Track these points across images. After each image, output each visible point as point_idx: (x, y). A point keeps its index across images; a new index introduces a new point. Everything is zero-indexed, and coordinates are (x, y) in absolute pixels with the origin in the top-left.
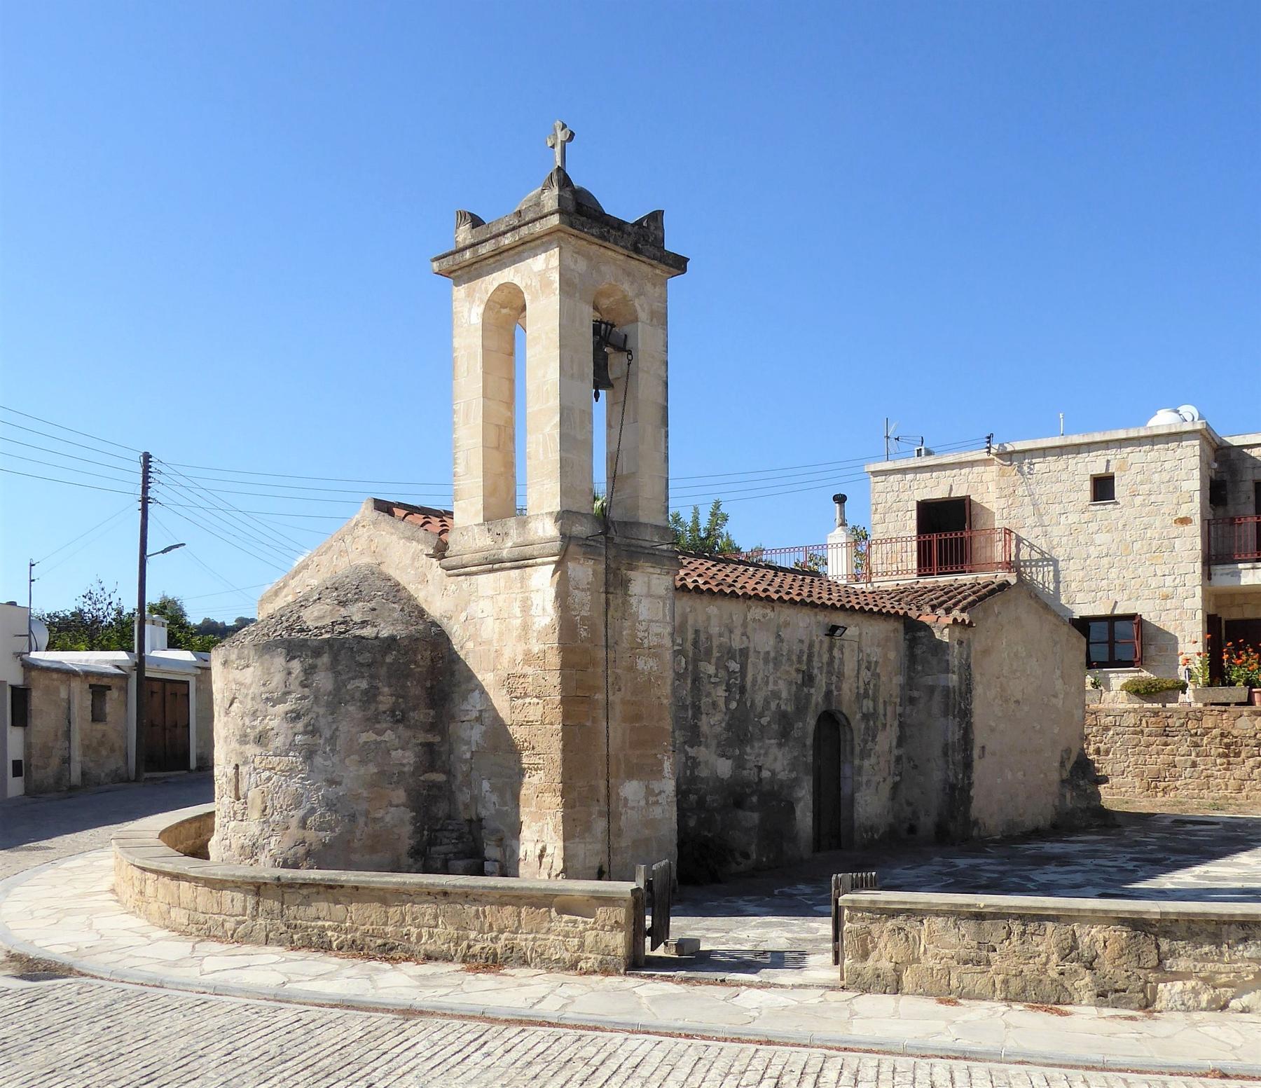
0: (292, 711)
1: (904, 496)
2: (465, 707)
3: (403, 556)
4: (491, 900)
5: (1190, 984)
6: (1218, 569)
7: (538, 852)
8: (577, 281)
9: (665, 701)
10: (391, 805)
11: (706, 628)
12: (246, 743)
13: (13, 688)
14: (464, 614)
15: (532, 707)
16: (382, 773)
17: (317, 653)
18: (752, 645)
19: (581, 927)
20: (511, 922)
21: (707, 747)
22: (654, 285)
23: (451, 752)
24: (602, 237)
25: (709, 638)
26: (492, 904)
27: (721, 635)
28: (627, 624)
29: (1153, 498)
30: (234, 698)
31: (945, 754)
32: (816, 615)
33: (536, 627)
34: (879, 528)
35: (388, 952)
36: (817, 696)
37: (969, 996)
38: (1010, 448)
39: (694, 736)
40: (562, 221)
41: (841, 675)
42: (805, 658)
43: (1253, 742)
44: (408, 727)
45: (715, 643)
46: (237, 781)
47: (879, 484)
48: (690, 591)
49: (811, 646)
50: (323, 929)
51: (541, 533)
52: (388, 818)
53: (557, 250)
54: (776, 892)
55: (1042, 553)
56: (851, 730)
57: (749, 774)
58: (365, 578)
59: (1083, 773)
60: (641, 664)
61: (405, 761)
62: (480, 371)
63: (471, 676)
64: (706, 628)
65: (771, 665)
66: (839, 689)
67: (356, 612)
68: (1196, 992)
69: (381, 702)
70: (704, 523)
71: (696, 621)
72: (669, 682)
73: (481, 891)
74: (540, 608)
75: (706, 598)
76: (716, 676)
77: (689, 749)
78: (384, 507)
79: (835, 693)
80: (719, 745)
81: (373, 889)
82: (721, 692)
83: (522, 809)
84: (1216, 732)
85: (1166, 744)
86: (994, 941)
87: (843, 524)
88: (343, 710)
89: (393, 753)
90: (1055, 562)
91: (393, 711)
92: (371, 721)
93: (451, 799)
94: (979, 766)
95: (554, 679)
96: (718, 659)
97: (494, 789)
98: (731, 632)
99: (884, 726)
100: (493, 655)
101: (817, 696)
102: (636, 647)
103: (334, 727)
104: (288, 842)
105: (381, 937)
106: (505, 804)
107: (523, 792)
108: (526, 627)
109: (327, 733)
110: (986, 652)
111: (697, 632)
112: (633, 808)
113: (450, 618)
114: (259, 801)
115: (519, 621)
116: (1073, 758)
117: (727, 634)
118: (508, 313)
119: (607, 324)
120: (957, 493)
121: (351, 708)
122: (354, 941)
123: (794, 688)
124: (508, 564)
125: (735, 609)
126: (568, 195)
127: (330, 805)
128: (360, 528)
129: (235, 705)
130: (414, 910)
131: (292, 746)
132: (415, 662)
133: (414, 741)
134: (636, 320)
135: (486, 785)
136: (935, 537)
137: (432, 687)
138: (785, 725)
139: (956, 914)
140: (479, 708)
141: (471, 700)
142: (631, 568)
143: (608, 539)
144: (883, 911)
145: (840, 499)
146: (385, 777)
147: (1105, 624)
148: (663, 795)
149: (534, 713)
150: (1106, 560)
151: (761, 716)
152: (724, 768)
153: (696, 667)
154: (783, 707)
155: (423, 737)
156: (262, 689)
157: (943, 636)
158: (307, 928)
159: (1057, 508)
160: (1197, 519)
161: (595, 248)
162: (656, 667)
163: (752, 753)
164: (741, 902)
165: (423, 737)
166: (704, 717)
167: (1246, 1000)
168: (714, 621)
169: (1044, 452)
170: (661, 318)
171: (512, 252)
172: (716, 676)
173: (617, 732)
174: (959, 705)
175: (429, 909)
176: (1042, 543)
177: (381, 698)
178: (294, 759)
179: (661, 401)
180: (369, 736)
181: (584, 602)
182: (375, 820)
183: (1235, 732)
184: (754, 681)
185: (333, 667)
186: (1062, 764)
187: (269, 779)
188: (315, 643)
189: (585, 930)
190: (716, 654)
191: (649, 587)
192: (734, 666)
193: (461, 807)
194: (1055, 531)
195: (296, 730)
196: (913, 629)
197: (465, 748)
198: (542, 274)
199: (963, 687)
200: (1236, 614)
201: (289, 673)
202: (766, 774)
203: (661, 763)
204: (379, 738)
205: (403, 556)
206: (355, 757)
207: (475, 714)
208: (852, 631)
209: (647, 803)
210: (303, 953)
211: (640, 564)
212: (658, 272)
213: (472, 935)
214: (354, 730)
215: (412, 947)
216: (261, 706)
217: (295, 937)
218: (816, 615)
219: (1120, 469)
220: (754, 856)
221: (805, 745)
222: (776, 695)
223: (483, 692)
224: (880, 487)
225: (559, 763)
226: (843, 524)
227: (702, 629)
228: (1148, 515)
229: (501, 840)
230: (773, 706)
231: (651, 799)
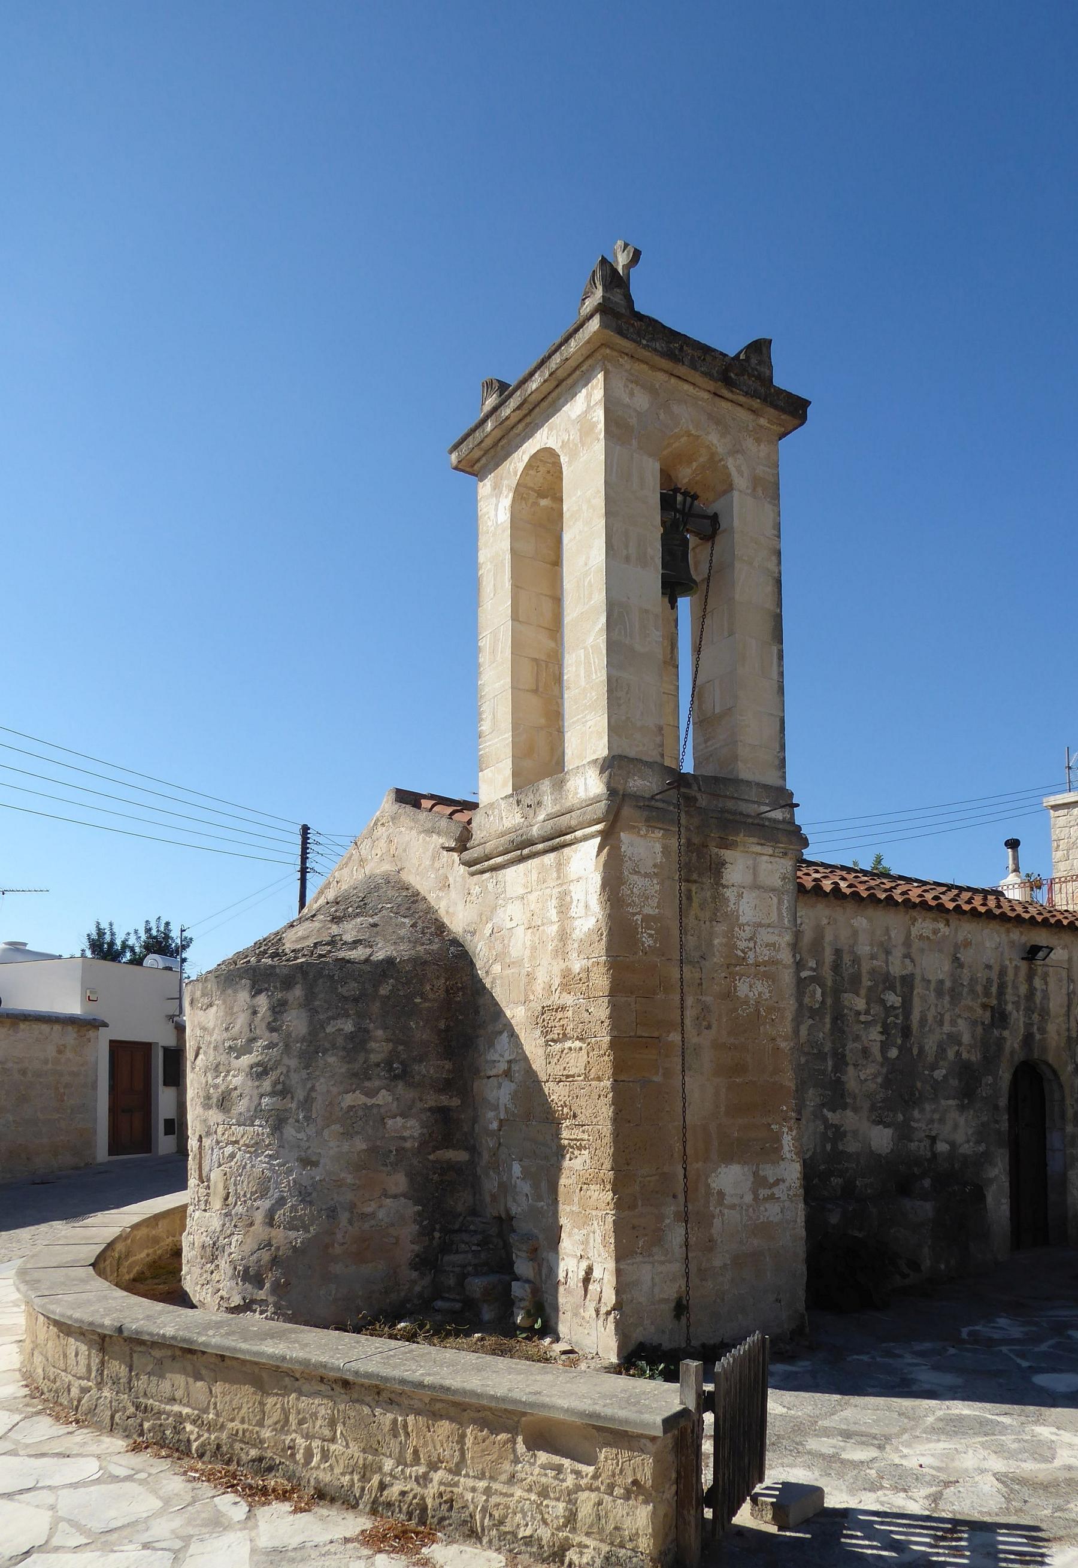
0: (258, 1064)
2: (492, 1056)
3: (420, 857)
4: (417, 1404)
7: (582, 1274)
8: (633, 421)
9: (783, 1045)
10: (386, 1196)
11: (852, 946)
12: (209, 1107)
13: (166, 1050)
14: (490, 925)
15: (573, 1055)
16: (373, 1150)
17: (288, 983)
18: (918, 971)
19: (570, 1481)
20: (448, 1452)
21: (855, 1110)
22: (758, 441)
23: (475, 1120)
25: (856, 960)
26: (418, 1413)
27: (873, 957)
30: (199, 1048)
32: (1008, 931)
33: (577, 934)
34: (1062, 866)
39: (836, 1096)
40: (603, 325)
41: (1044, 1013)
42: (994, 989)
44: (410, 1085)
45: (865, 967)
46: (201, 1158)
47: (1060, 819)
48: (826, 894)
49: (1002, 973)
50: (180, 1418)
51: (582, 794)
52: (381, 1214)
53: (600, 376)
54: (965, 1332)
56: (1061, 1086)
57: (917, 1147)
58: (377, 888)
60: (743, 989)
61: (406, 1134)
62: (508, 586)
63: (498, 1013)
64: (852, 946)
65: (947, 998)
66: (1042, 1030)
67: (349, 931)
69: (372, 1051)
71: (836, 937)
72: (789, 1015)
73: (398, 1387)
74: (582, 905)
75: (850, 907)
76: (867, 1012)
77: (829, 1115)
78: (408, 799)
79: (1038, 1037)
80: (873, 1108)
81: (244, 1362)
82: (875, 1035)
83: (561, 1207)
87: (1016, 870)
88: (321, 1062)
89: (390, 1122)
91: (389, 1064)
92: (359, 1078)
93: (475, 1186)
95: (601, 1011)
96: (870, 989)
97: (526, 1174)
98: (888, 953)
100: (524, 980)
101: (1012, 1040)
102: (735, 963)
103: (309, 1086)
104: (250, 1244)
105: (254, 1446)
106: (539, 1198)
107: (563, 1181)
108: (563, 936)
109: (300, 1094)
111: (838, 952)
112: (733, 1207)
113: (473, 933)
114: (221, 1186)
115: (555, 928)
117: (882, 956)
118: (542, 493)
119: (685, 494)
121: (331, 1060)
122: (219, 1447)
123: (979, 1030)
124: (540, 846)
125: (894, 923)
127: (304, 1194)
128: (380, 828)
129: (201, 1057)
130: (301, 1406)
131: (258, 1111)
132: (422, 995)
133: (419, 1105)
134: (730, 488)
135: (517, 1169)
137: (448, 1029)
138: (968, 1082)
140: (507, 1057)
141: (498, 1047)
142: (726, 844)
143: (692, 808)
145: (1013, 844)
146: (378, 1156)
148: (782, 1186)
149: (576, 1063)
151: (934, 1067)
152: (881, 1139)
153: (837, 1000)
154: (965, 1056)
156: (225, 1035)
158: (160, 1413)
161: (661, 377)
163: (921, 1119)
164: (909, 1359)
165: (432, 1100)
166: (851, 1069)
168: (863, 938)
171: (544, 404)
172: (867, 1012)
173: (701, 1093)
175: (322, 1407)
177: (373, 1045)
178: (259, 1129)
179: (770, 605)
181: (649, 894)
182: (364, 1216)
184: (923, 1021)
185: (308, 1003)
187: (232, 1156)
188: (285, 971)
189: (578, 1488)
190: (866, 982)
191: (755, 875)
192: (893, 999)
193: (488, 1199)
195: (262, 1090)
197: (491, 1114)
198: (583, 419)
201: (255, 1013)
202: (942, 1147)
203: (777, 1138)
204: (370, 1102)
205: (420, 857)
206: (336, 1128)
207: (503, 1066)
208: (1059, 955)
209: (756, 1198)
211: (740, 838)
212: (762, 421)
213: (388, 1464)
214: (335, 1090)
215: (300, 1471)
216: (223, 1058)
217: (146, 1425)
218: (1008, 931)
220: (928, 1263)
221: (996, 1107)
222: (954, 1039)
223: (513, 1035)
224: (1062, 821)
225: (608, 1139)
226: (1016, 870)
227: (846, 948)
229: (536, 1250)
230: (951, 1054)
231: (763, 1192)
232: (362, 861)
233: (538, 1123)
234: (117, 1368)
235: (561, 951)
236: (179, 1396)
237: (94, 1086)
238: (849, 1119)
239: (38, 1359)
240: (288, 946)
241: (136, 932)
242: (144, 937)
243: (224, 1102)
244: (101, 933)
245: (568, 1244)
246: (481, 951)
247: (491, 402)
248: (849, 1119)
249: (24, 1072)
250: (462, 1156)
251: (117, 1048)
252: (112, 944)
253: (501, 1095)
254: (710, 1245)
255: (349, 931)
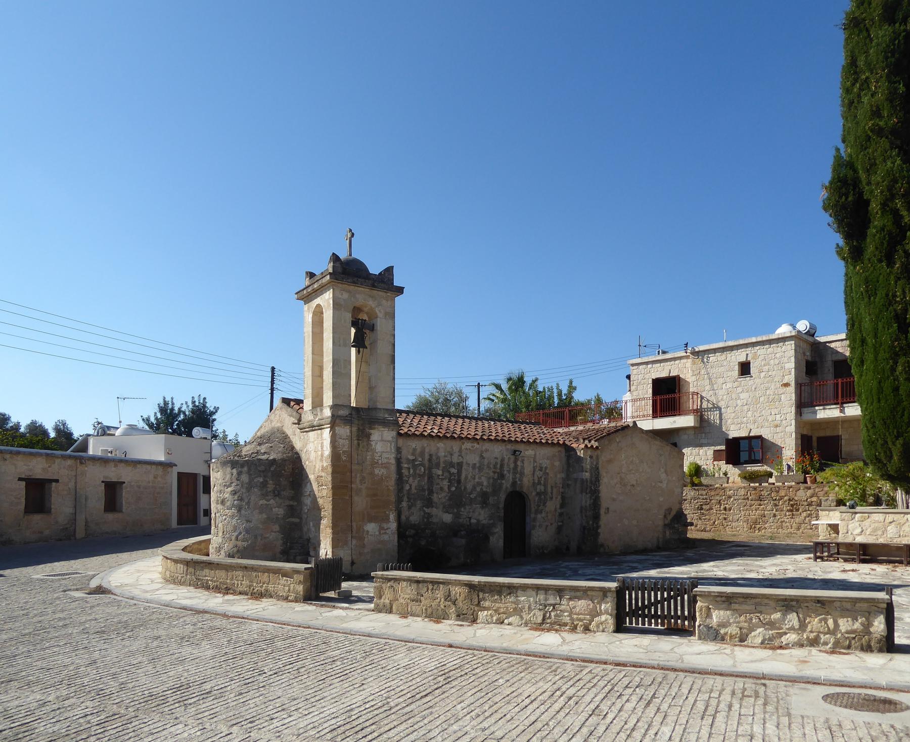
1: (647, 376)
5: (490, 612)
6: (805, 410)
13: (204, 476)
17: (242, 466)
20: (267, 580)
23: (301, 509)
24: (354, 282)
25: (438, 458)
27: (445, 456)
28: (369, 454)
29: (770, 373)
31: (581, 512)
35: (227, 591)
36: (507, 484)
37: (413, 615)
38: (697, 350)
41: (522, 474)
42: (498, 466)
43: (806, 503)
45: (442, 460)
49: (503, 460)
55: (713, 404)
59: (679, 520)
60: (377, 471)
66: (521, 480)
68: (492, 616)
70: (565, 391)
75: (436, 440)
80: (444, 507)
82: (445, 483)
84: (786, 498)
85: (760, 505)
86: (422, 592)
90: (720, 409)
92: (264, 496)
94: (604, 519)
95: (330, 478)
98: (451, 455)
99: (552, 498)
102: (374, 464)
108: (322, 455)
109: (246, 501)
110: (610, 461)
116: (673, 513)
120: (673, 374)
123: (491, 481)
125: (456, 446)
126: (338, 264)
136: (658, 398)
139: (410, 580)
144: (386, 579)
147: (747, 441)
150: (745, 408)
151: (471, 493)
152: (448, 518)
155: (288, 503)
157: (581, 454)
159: (721, 381)
160: (793, 384)
162: (386, 472)
163: (464, 512)
165: (288, 503)
166: (435, 495)
167: (510, 620)
169: (715, 351)
170: (391, 315)
173: (360, 502)
174: (593, 488)
175: (240, 573)
176: (713, 399)
178: (234, 510)
179: (391, 353)
180: (263, 502)
181: (344, 445)
183: (796, 498)
184: (466, 477)
185: (249, 472)
186: (665, 516)
190: (442, 465)
192: (453, 470)
194: (721, 393)
196: (569, 450)
199: (593, 479)
200: (822, 434)
202: (473, 521)
203: (388, 516)
210: (200, 590)
219: (753, 358)
228: (768, 382)
230: (478, 489)
231: (382, 532)
232: (271, 421)
233: (316, 508)
234: (191, 570)
235: (321, 460)
236: (207, 575)
237: (171, 493)
238: (434, 511)
239: (168, 573)
240: (243, 453)
241: (186, 403)
242: (191, 406)
243: (223, 502)
244: (166, 403)
245: (322, 545)
246: (303, 457)
247: (307, 283)
248: (434, 511)
249: (139, 487)
250: (297, 520)
251: (181, 475)
252: (172, 409)
253: (308, 501)
254: (364, 546)
255: (263, 449)
